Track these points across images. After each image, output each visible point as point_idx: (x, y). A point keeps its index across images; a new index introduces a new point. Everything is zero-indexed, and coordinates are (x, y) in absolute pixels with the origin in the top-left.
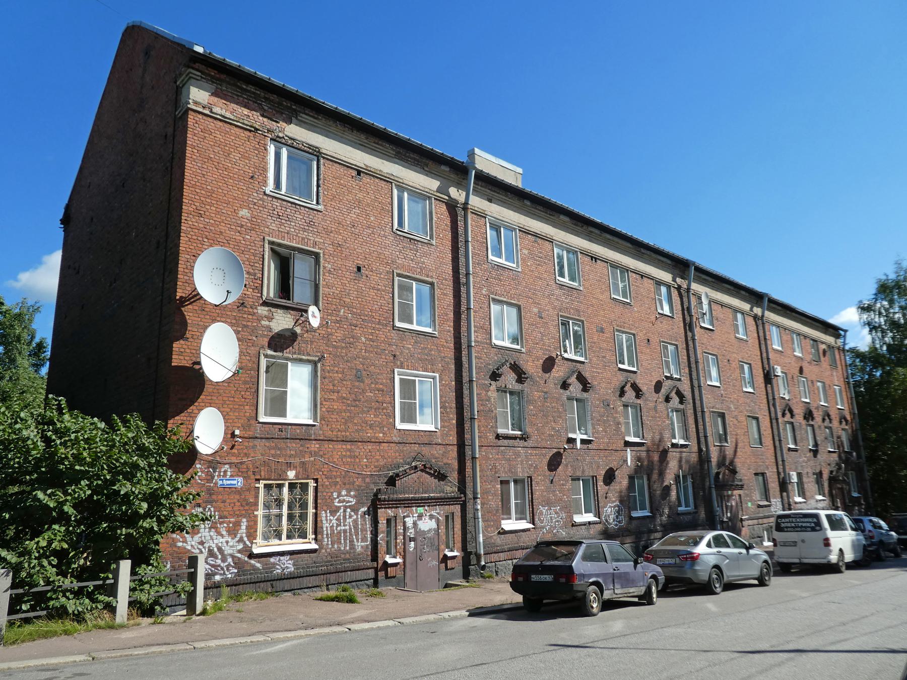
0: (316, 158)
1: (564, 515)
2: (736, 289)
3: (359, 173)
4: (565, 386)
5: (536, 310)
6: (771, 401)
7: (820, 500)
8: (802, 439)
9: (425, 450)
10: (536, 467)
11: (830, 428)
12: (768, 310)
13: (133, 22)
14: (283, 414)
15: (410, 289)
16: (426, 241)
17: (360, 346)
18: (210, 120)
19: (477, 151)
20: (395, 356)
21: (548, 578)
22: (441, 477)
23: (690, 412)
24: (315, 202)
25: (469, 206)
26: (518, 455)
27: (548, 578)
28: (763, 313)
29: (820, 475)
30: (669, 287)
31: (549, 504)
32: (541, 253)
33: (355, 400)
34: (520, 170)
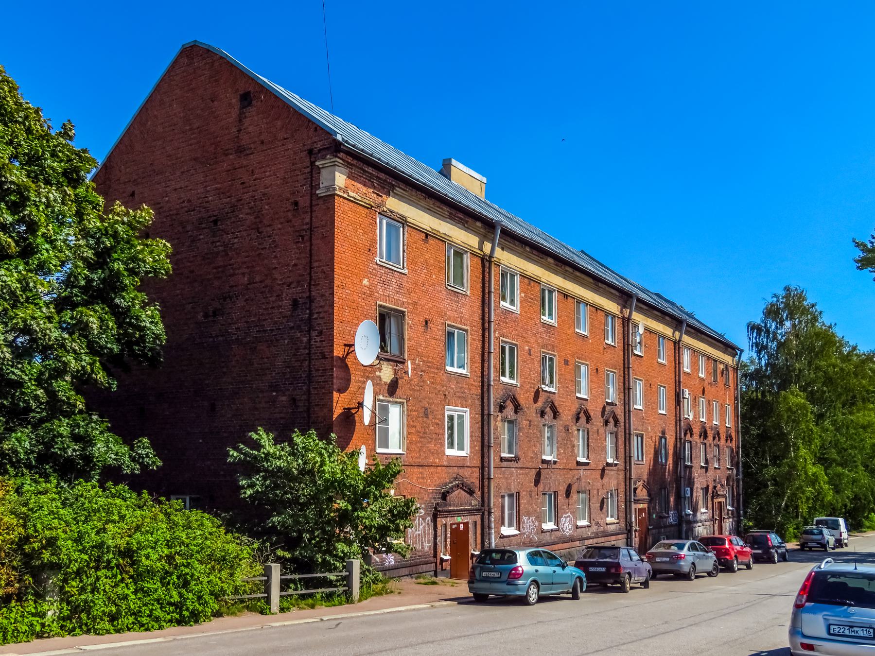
0: (401, 225)
1: (537, 524)
2: (663, 316)
3: (427, 235)
4: (542, 414)
5: (527, 348)
6: (678, 419)
7: (704, 513)
8: (696, 457)
9: (461, 472)
10: (522, 484)
11: (718, 446)
12: (685, 334)
13: (196, 41)
14: (387, 447)
15: (453, 334)
16: (464, 293)
17: (427, 389)
18: (346, 202)
19: (454, 162)
20: (445, 395)
21: (603, 569)
22: (471, 493)
23: (621, 434)
24: (401, 267)
25: (493, 260)
26: (512, 474)
27: (603, 569)
28: (681, 337)
29: (707, 489)
30: (614, 316)
31: (529, 514)
32: (532, 294)
33: (424, 433)
34: (485, 180)
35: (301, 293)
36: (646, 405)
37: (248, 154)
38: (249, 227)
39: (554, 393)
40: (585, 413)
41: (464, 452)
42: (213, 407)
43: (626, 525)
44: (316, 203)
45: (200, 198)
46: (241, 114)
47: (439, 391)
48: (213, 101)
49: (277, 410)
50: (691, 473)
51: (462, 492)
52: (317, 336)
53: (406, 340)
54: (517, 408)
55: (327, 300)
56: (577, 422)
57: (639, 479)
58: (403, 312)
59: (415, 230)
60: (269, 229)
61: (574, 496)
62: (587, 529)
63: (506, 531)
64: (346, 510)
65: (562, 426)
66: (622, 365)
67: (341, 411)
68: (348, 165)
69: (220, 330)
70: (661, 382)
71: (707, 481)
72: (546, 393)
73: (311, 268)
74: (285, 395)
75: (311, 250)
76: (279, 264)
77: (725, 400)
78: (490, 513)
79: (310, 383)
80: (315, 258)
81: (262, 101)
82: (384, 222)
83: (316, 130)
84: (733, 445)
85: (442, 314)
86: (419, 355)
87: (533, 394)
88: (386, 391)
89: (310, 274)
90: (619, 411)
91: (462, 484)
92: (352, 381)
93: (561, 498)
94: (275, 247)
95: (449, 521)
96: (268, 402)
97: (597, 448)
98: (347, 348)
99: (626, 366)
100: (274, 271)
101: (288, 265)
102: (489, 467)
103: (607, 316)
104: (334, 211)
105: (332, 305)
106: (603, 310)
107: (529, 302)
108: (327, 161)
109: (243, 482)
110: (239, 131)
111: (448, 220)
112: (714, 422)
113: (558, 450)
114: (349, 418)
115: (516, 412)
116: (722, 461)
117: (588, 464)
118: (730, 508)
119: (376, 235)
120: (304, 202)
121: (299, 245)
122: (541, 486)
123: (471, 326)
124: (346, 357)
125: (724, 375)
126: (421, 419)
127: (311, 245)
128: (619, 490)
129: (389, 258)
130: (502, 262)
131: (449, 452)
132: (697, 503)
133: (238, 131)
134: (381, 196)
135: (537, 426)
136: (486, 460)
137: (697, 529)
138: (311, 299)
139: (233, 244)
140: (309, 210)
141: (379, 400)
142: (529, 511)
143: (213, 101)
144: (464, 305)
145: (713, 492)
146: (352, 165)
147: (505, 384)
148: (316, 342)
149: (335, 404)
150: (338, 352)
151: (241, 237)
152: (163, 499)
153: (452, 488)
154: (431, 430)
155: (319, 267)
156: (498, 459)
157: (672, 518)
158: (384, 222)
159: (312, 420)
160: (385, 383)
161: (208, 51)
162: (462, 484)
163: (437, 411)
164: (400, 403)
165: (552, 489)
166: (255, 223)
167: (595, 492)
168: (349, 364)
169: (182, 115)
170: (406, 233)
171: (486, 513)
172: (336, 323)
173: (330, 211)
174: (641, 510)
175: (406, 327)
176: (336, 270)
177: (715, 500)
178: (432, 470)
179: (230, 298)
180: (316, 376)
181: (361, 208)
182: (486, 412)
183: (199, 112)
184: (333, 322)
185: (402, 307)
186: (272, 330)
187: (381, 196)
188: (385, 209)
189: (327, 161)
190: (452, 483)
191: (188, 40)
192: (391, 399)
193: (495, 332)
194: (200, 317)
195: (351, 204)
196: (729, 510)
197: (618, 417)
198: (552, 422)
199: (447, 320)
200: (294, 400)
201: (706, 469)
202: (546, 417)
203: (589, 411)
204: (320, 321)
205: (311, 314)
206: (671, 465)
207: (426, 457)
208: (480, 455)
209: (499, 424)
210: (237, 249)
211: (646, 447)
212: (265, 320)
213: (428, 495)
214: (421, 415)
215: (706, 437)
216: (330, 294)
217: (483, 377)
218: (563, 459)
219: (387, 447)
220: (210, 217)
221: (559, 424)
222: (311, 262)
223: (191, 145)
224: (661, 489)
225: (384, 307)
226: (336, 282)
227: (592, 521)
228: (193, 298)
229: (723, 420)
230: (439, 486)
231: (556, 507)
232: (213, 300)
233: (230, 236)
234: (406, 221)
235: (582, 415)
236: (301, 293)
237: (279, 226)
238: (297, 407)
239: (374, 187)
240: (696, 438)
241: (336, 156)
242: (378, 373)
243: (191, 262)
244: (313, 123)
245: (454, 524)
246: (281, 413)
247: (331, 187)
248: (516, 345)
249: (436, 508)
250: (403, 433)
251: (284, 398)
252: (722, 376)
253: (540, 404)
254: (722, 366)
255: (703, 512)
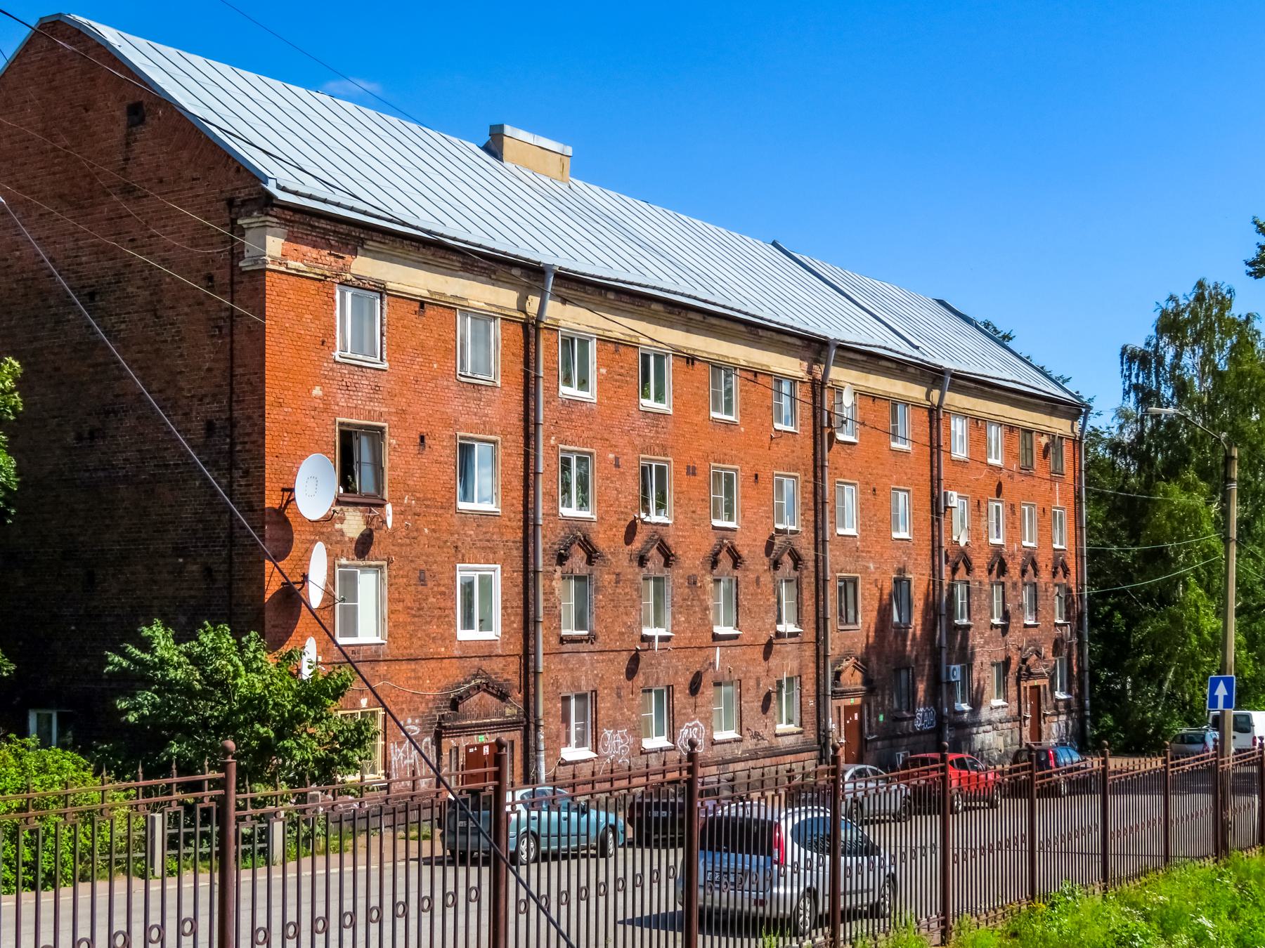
3: (422, 304)
4: (642, 561)
5: (611, 456)
7: (998, 708)
9: (486, 665)
13: (60, 14)
14: (355, 635)
17: (423, 540)
18: (284, 277)
19: (508, 130)
20: (456, 547)
22: (503, 697)
25: (542, 325)
26: (582, 662)
29: (1007, 663)
30: (794, 381)
31: (615, 725)
33: (419, 609)
34: (569, 151)
35: (218, 411)
36: (863, 527)
37: (140, 197)
38: (142, 307)
39: (667, 525)
40: (729, 551)
41: (493, 633)
42: (91, 578)
43: (819, 736)
44: (239, 279)
45: (69, 257)
46: (128, 135)
47: (447, 541)
48: (87, 111)
49: (185, 585)
50: (965, 638)
51: (487, 696)
52: (241, 477)
53: (386, 470)
54: (592, 555)
55: (256, 425)
56: (713, 568)
57: (847, 656)
58: (381, 429)
59: (401, 300)
60: (171, 313)
61: (708, 691)
62: (735, 745)
63: (571, 753)
64: (268, 738)
65: (682, 577)
66: (811, 462)
67: (277, 588)
68: (287, 222)
69: (100, 461)
70: (897, 484)
71: (1007, 650)
72: (650, 527)
73: (232, 376)
74: (197, 564)
75: (232, 349)
76: (186, 366)
77: (1051, 501)
78: (537, 727)
79: (232, 546)
80: (238, 361)
81: (159, 119)
82: (349, 295)
83: (238, 170)
84: (1072, 581)
85: (450, 422)
86: (411, 491)
87: (624, 530)
88: (352, 551)
89: (231, 384)
90: (805, 547)
91: (487, 684)
92: (296, 542)
93: (681, 697)
94: (180, 340)
95: (463, 742)
96: (172, 573)
97: (756, 609)
98: (287, 494)
99: (819, 463)
100: (179, 377)
101: (200, 369)
102: (536, 654)
103: (779, 382)
104: (265, 294)
105: (262, 433)
106: (769, 374)
107: (616, 381)
108: (253, 220)
109: (123, 705)
110: (127, 160)
111: (461, 273)
112: (1026, 543)
113: (674, 618)
114: (291, 597)
115: (590, 562)
116: (1043, 612)
117: (737, 637)
118: (1060, 695)
119: (334, 319)
120: (222, 276)
121: (215, 340)
122: (640, 679)
123: (504, 433)
124: (285, 508)
125: (1051, 455)
126: (413, 588)
127: (232, 342)
128: (804, 677)
129: (358, 348)
130: (562, 323)
131: (463, 635)
132: (981, 691)
133: (124, 160)
134: (343, 258)
135: (633, 582)
136: (531, 643)
137: (981, 736)
138: (232, 422)
139: (120, 331)
140: (229, 290)
141: (340, 566)
142: (615, 720)
143: (87, 111)
144: (489, 403)
145: (1020, 669)
146: (291, 221)
147: (568, 519)
148: (241, 486)
149: (267, 579)
150: (272, 500)
151: (130, 321)
152: (12, 736)
153: (467, 691)
154: (431, 603)
155: (244, 375)
156: (554, 641)
157: (922, 718)
158: (349, 295)
159: (234, 602)
160: (351, 540)
161: (79, 32)
162: (487, 684)
163: (442, 573)
164: (377, 566)
165: (661, 682)
166: (151, 302)
167: (752, 683)
168: (290, 517)
169: (40, 126)
170: (385, 307)
171: (532, 726)
172: (269, 460)
173: (258, 293)
174: (849, 710)
175: (386, 451)
176: (268, 381)
177: (1023, 684)
178: (433, 664)
179: (115, 413)
180: (241, 537)
181: (308, 282)
182: (531, 567)
183: (66, 124)
184: (263, 457)
185: (379, 421)
186: (177, 465)
187: (343, 258)
188: (349, 277)
189: (253, 220)
190: (469, 682)
191: (48, 11)
192: (361, 563)
193: (548, 437)
194: (70, 439)
195: (293, 279)
196: (1058, 700)
197: (802, 552)
198: (662, 571)
199: (459, 430)
200: (208, 572)
201: (1005, 629)
202: (650, 565)
203: (738, 548)
204: (246, 456)
205: (232, 445)
206: (919, 628)
207: (421, 646)
208: (521, 635)
209: (557, 584)
210: (124, 338)
211: (864, 598)
212: (166, 449)
213: (427, 704)
214: (412, 582)
215: (1003, 570)
216: (260, 416)
217: (526, 511)
218: (684, 632)
219: (355, 635)
220: (83, 287)
221: (674, 577)
222: (232, 368)
223: (54, 174)
224: (897, 671)
225: (349, 425)
226: (269, 399)
227: (744, 732)
228: (60, 409)
229: (1045, 534)
230: (446, 688)
231: (671, 711)
232: (90, 414)
233: (114, 319)
234: (384, 288)
235: (724, 553)
236: (218, 411)
237: (186, 310)
238: (214, 581)
239: (331, 247)
240: (980, 574)
241: (267, 214)
242: (338, 526)
243: (55, 354)
244: (234, 161)
245: (473, 747)
246: (191, 589)
247: (259, 258)
248: (591, 454)
249: (439, 723)
250: (382, 612)
251: (195, 568)
252: (1045, 457)
253: (637, 544)
254: (1044, 440)
255: (995, 705)
